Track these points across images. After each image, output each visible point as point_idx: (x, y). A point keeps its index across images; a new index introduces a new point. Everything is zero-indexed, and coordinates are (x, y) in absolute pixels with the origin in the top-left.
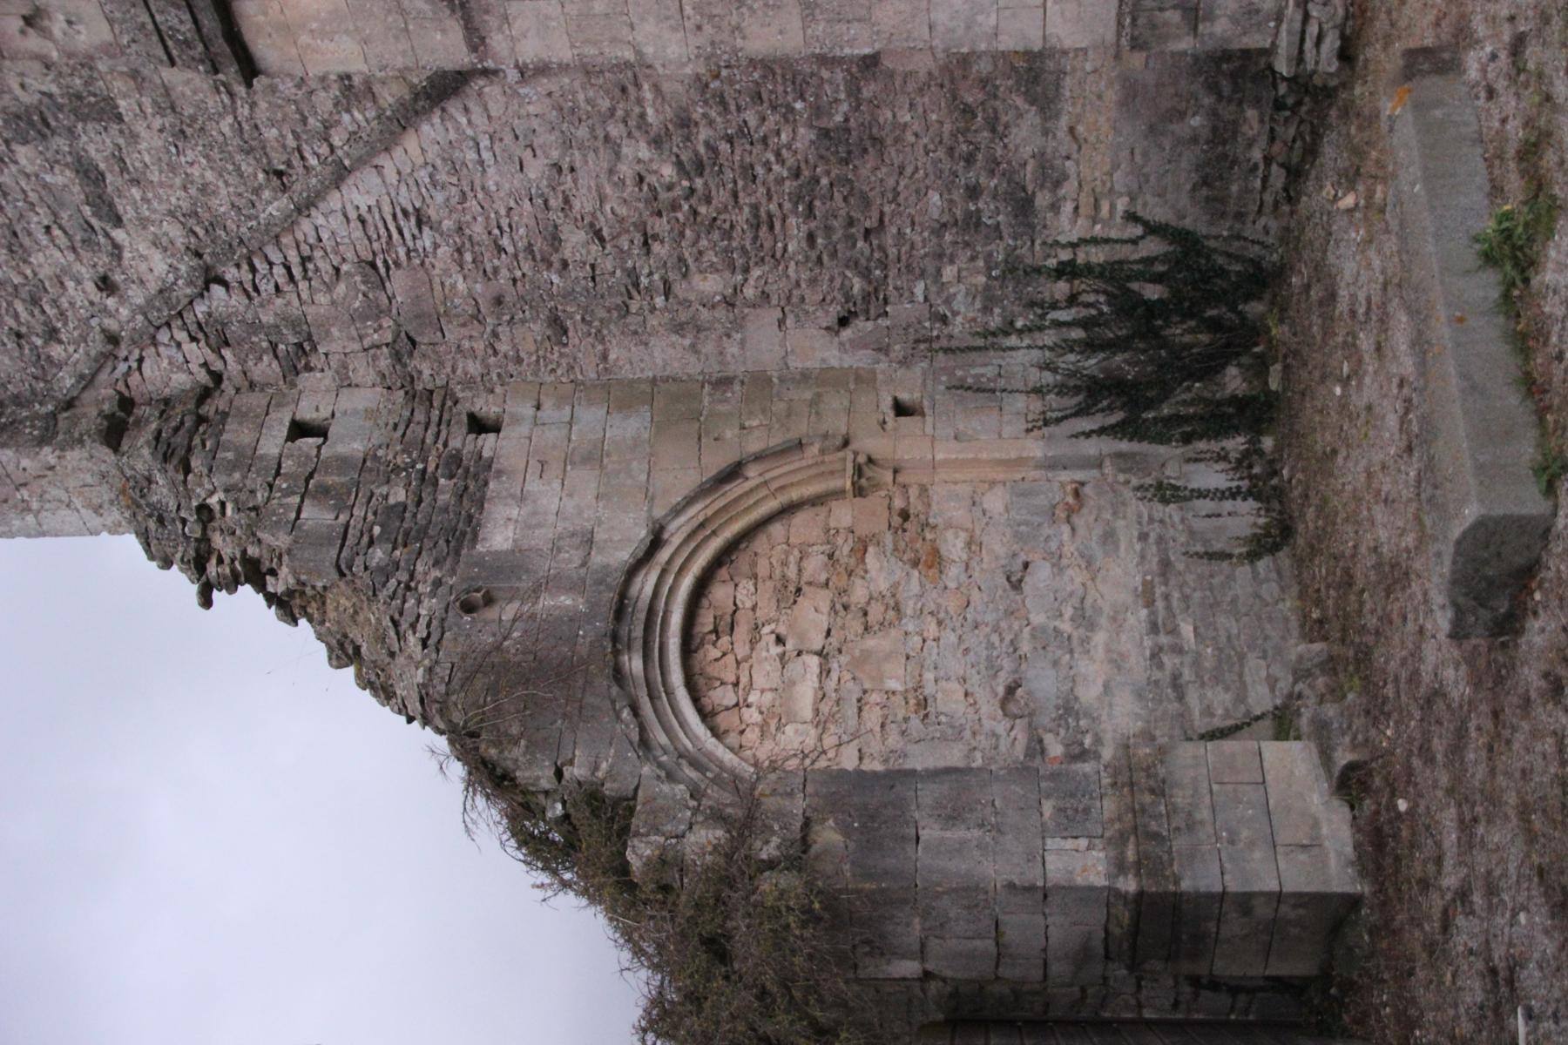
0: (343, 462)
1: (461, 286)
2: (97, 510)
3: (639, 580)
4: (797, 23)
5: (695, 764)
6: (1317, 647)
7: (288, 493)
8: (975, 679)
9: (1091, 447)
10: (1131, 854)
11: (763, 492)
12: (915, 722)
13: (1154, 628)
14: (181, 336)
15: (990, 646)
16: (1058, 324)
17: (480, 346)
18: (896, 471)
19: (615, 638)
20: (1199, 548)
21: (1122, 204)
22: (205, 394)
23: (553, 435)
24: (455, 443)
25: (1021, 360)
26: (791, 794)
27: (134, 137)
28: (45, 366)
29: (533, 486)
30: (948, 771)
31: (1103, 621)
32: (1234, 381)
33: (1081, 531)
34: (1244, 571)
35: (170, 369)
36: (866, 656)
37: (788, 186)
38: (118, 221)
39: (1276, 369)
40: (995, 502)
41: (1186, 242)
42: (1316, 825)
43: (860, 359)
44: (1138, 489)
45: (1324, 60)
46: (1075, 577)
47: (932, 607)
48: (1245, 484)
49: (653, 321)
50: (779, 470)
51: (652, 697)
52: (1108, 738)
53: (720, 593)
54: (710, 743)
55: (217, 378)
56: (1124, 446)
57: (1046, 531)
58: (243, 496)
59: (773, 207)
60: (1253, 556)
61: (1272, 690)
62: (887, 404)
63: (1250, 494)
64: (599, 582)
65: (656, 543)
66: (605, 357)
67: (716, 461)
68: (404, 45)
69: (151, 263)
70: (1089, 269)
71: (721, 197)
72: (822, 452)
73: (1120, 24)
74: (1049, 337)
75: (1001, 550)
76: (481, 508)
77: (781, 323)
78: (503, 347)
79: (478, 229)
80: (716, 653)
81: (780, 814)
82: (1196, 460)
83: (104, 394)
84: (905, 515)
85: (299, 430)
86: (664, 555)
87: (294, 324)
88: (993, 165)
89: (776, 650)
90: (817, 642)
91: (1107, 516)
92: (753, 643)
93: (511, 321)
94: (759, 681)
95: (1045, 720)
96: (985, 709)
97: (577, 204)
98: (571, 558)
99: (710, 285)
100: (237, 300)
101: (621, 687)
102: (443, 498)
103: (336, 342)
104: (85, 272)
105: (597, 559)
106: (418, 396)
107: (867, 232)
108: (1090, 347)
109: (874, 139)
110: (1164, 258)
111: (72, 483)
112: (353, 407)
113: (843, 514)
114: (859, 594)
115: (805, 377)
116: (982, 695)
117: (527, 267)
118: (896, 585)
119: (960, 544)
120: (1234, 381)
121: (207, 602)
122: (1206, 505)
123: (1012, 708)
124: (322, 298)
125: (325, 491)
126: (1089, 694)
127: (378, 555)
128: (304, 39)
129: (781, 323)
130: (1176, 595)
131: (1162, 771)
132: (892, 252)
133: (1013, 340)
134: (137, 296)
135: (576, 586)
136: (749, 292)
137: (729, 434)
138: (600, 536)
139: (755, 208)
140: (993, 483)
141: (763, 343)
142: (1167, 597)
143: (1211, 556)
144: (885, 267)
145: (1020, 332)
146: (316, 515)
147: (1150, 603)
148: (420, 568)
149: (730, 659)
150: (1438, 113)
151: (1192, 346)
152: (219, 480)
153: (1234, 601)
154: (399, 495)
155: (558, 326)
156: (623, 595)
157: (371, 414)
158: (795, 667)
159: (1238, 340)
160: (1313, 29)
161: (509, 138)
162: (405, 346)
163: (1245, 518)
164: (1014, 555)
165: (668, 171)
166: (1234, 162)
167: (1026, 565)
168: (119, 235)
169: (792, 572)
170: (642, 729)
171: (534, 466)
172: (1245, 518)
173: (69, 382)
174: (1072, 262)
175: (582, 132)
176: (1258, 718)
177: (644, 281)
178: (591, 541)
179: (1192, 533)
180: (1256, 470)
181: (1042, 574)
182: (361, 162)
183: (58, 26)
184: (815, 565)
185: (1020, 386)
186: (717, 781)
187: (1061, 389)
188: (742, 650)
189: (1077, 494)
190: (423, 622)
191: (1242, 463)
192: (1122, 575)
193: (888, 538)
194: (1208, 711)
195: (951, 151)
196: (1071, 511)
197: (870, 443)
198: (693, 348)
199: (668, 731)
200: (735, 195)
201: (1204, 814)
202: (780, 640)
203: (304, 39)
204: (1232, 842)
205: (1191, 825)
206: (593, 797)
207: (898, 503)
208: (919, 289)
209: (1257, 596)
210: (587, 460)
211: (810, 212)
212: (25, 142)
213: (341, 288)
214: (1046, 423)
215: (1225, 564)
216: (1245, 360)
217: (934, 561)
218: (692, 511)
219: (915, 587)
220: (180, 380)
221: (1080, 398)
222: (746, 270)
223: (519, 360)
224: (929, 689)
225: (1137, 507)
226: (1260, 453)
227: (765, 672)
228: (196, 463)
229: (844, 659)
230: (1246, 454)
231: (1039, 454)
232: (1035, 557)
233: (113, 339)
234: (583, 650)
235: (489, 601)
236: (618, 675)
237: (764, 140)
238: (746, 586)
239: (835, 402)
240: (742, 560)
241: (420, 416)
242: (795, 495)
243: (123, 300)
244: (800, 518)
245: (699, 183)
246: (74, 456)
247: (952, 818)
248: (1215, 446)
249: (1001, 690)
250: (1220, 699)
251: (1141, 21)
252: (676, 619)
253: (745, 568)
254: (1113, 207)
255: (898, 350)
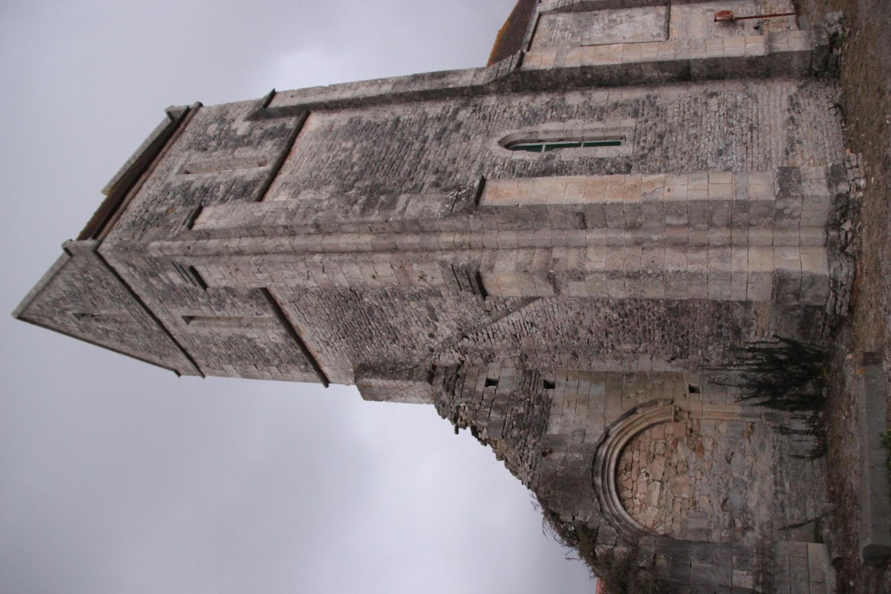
0: (503, 397)
1: (544, 342)
2: (424, 398)
3: (601, 449)
4: (663, 291)
5: (618, 520)
6: (830, 505)
7: (486, 407)
8: (713, 496)
9: (758, 410)
10: (761, 579)
11: (643, 419)
12: (692, 510)
13: (776, 484)
14: (453, 351)
15: (719, 484)
16: (748, 364)
17: (548, 359)
18: (689, 413)
19: (592, 471)
20: (793, 453)
21: (772, 333)
22: (459, 367)
23: (573, 391)
24: (539, 392)
25: (735, 373)
26: (650, 545)
27: (445, 301)
28: (411, 355)
29: (566, 410)
30: (702, 542)
31: (758, 478)
32: (810, 389)
33: (753, 442)
34: (809, 464)
35: (449, 359)
36: (676, 484)
37: (656, 322)
38: (437, 320)
39: (825, 389)
40: (723, 428)
41: (794, 344)
42: (824, 575)
43: (678, 370)
44: (774, 428)
45: (844, 311)
46: (750, 459)
47: (699, 467)
48: (811, 429)
49: (607, 356)
50: (649, 412)
51: (604, 493)
52: (757, 523)
53: (627, 455)
54: (623, 512)
55: (463, 362)
56: (769, 410)
57: (741, 441)
58: (471, 405)
59: (651, 327)
60: (812, 458)
61: (815, 510)
62: (687, 387)
63: (814, 433)
64: (588, 449)
65: (607, 436)
66: (590, 365)
67: (628, 407)
68: (534, 290)
69: (445, 330)
70: (760, 350)
71: (633, 324)
72: (664, 405)
73: (772, 294)
74: (745, 368)
75: (724, 447)
76: (548, 418)
77: (651, 358)
78: (556, 360)
79: (551, 328)
80: (625, 478)
81: (647, 552)
82: (795, 418)
83: (428, 364)
84: (691, 431)
85: (489, 382)
86: (609, 441)
87: (489, 350)
88: (727, 320)
89: (646, 478)
90: (660, 477)
91: (762, 437)
92: (638, 475)
93: (560, 353)
94: (640, 490)
95: (735, 514)
96: (716, 508)
97: (584, 323)
98: (578, 439)
99: (628, 347)
100: (471, 343)
101: (594, 489)
102: (536, 413)
103: (502, 356)
104: (426, 333)
105: (587, 441)
106: (528, 373)
107: (682, 336)
108: (759, 371)
109: (687, 312)
110: (787, 348)
111: (416, 390)
112: (506, 373)
113: (670, 429)
114: (674, 460)
115: (658, 375)
116: (715, 502)
117: (566, 338)
118: (687, 458)
119: (710, 443)
120: (810, 389)
121: (457, 432)
122: (797, 437)
123: (725, 508)
124: (498, 343)
125: (497, 407)
126: (752, 505)
127: (515, 432)
128: (503, 288)
129: (651, 358)
130: (784, 471)
131: (773, 550)
132: (691, 341)
133: (732, 368)
134: (440, 339)
135: (580, 450)
136: (641, 349)
137: (632, 396)
138: (588, 432)
139: (644, 327)
140: (722, 421)
141: (645, 364)
142: (781, 472)
143: (798, 457)
144: (688, 345)
145: (735, 366)
146: (495, 416)
147: (775, 474)
148: (529, 438)
149: (630, 480)
150: (873, 381)
151: (795, 373)
152: (464, 400)
153: (805, 474)
154: (521, 410)
155: (575, 356)
156: (595, 455)
157: (512, 378)
158: (651, 486)
159: (812, 374)
160: (839, 303)
161: (563, 305)
162: (523, 358)
163: (810, 443)
164: (729, 450)
165: (615, 316)
166: (812, 324)
167: (733, 454)
168: (437, 324)
169: (652, 450)
170: (601, 505)
171: (566, 403)
172: (810, 443)
173: (417, 361)
174: (754, 348)
175: (588, 305)
176: (809, 521)
177: (605, 345)
178: (584, 434)
179: (792, 447)
180: (816, 424)
181: (737, 458)
182: (514, 310)
183: (429, 279)
184: (660, 448)
185: (733, 383)
186: (625, 527)
187: (749, 386)
188: (634, 478)
189: (752, 427)
190: (530, 459)
191: (811, 421)
192: (766, 461)
193: (685, 439)
194: (792, 517)
195: (713, 316)
196: (749, 433)
197: (680, 403)
198: (621, 364)
199: (609, 506)
200: (638, 324)
201: (786, 567)
202: (647, 475)
203: (503, 288)
204: (795, 579)
205: (782, 571)
206: (584, 526)
207: (689, 426)
208: (700, 352)
209: (813, 474)
210: (583, 402)
211: (663, 329)
212: (413, 300)
213: (505, 341)
214: (742, 399)
215: (802, 461)
216: (814, 380)
217: (699, 449)
218: (619, 425)
219: (694, 459)
220: (451, 362)
221: (753, 391)
222: (640, 344)
223: (561, 364)
224: (697, 498)
225: (772, 434)
226: (818, 418)
227: (641, 487)
228: (457, 392)
229: (669, 484)
230: (813, 417)
231: (739, 411)
232: (736, 451)
233: (432, 350)
234: (582, 474)
235: (551, 452)
236: (593, 485)
237: (649, 310)
238: (636, 453)
239: (669, 386)
240: (635, 443)
241: (528, 380)
242: (654, 421)
243: (436, 340)
244: (655, 429)
245: (626, 320)
246: (418, 384)
247: (703, 560)
248: (802, 413)
249: (721, 501)
250: (797, 512)
251: (780, 297)
252: (613, 465)
253: (636, 446)
254: (769, 334)
255: (691, 368)
